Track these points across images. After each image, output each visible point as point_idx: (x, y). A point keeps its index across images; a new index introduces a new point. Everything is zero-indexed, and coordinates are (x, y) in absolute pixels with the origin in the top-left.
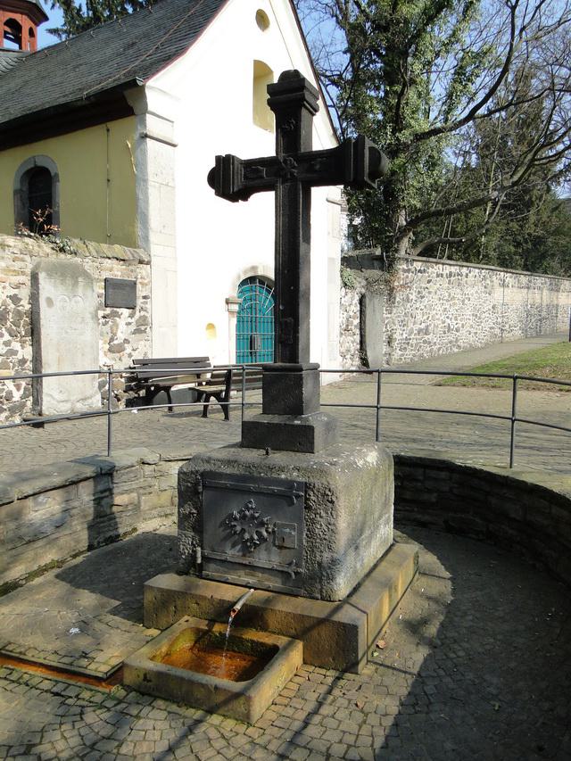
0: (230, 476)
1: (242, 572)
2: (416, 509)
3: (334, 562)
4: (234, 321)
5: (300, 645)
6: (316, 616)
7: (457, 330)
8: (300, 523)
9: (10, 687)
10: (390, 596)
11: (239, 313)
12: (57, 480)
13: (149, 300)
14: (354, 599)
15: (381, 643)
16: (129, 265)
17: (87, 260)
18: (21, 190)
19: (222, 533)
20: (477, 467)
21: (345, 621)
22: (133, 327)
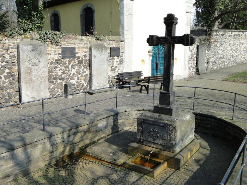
0: (151, 121)
1: (153, 144)
2: (204, 129)
3: (176, 144)
4: (151, 58)
5: (166, 163)
6: (170, 156)
7: (236, 57)
8: (168, 134)
9: (100, 165)
10: (191, 153)
11: (153, 55)
12: (105, 116)
13: (123, 53)
14: (180, 153)
15: (187, 164)
16: (118, 42)
17: (105, 42)
18: (83, 15)
19: (148, 134)
20: (222, 119)
21: (177, 158)
22: (118, 62)
